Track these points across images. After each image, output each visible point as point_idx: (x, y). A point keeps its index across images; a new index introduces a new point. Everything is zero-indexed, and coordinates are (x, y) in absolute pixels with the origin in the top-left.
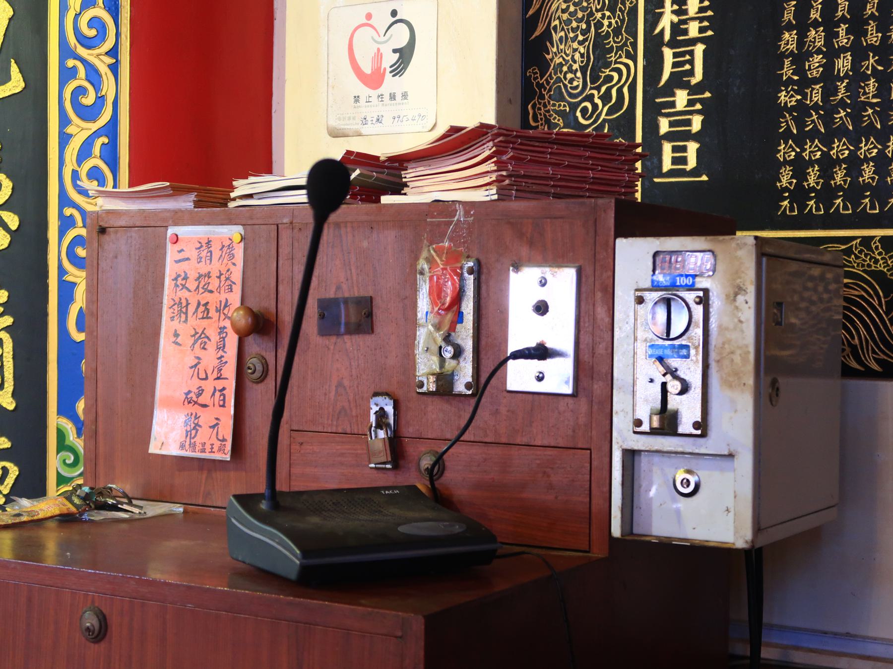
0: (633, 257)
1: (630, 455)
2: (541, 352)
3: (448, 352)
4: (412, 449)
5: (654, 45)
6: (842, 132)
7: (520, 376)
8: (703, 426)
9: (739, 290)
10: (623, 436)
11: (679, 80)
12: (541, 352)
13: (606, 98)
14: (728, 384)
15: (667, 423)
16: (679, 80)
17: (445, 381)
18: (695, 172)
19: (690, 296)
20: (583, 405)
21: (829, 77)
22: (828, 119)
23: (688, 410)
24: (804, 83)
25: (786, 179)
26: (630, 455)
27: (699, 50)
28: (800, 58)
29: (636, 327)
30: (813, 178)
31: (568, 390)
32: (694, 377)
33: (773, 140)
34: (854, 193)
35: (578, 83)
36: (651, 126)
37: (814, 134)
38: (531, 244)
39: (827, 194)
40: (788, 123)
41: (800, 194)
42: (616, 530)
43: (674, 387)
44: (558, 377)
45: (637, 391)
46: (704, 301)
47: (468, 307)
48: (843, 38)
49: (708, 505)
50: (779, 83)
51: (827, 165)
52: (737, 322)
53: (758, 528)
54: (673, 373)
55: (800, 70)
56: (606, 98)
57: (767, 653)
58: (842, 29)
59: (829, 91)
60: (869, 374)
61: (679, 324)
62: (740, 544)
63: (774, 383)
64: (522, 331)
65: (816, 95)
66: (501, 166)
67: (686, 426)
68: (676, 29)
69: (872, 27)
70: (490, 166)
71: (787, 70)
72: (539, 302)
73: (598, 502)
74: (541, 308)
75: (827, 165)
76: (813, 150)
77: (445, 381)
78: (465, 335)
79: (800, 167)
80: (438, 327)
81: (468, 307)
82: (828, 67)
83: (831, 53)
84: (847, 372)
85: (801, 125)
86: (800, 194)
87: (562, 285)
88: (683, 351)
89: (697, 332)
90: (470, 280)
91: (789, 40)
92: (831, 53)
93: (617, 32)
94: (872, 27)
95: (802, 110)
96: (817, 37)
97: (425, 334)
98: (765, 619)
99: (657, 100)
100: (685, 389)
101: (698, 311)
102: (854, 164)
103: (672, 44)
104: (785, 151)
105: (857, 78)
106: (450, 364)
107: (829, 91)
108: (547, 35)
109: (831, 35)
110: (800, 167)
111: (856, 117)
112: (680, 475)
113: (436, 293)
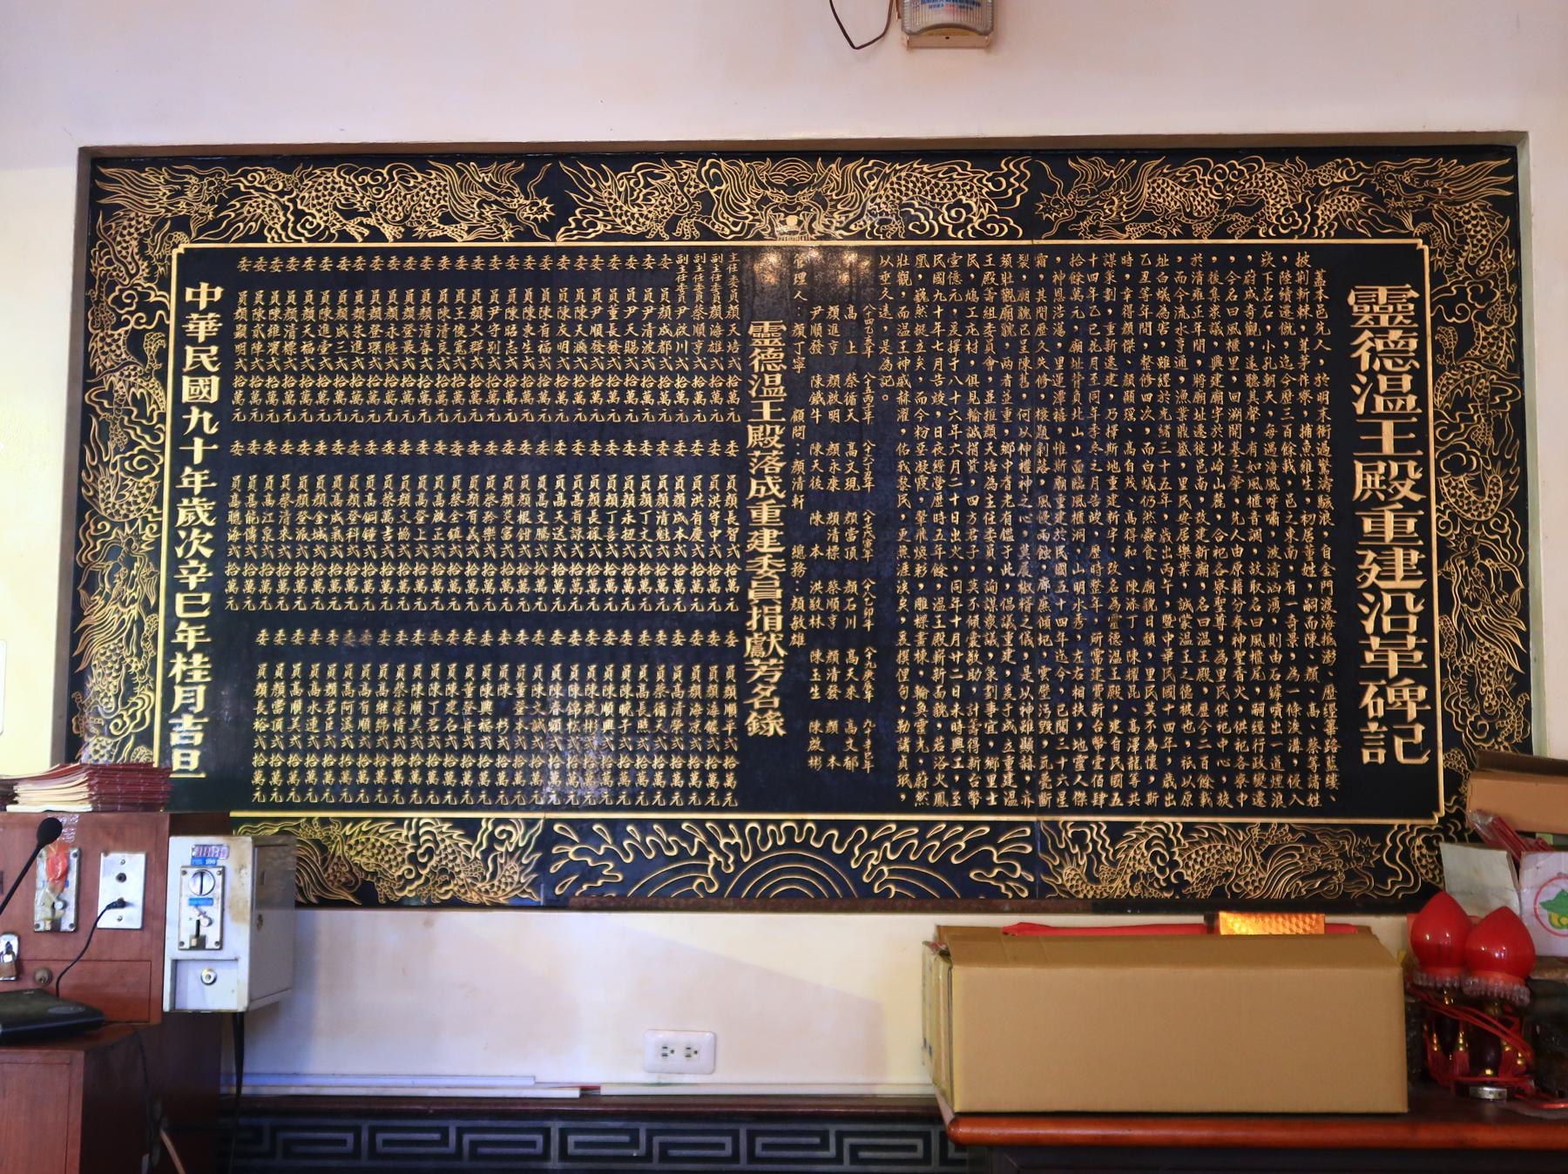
0: (181, 848)
1: (176, 962)
2: (121, 904)
3: (59, 905)
4: (28, 967)
5: (169, 684)
6: (294, 749)
7: (108, 921)
8: (220, 944)
9: (242, 867)
10: (172, 951)
11: (185, 708)
12: (121, 904)
13: (133, 717)
14: (235, 918)
15: (200, 943)
16: (185, 708)
17: (56, 924)
18: (197, 771)
19: (215, 871)
20: (147, 935)
21: (287, 714)
22: (286, 741)
23: (212, 935)
24: (271, 717)
25: (258, 778)
26: (176, 962)
27: (201, 690)
28: (269, 701)
29: (181, 887)
30: (276, 778)
31: (138, 925)
32: (216, 916)
33: (251, 752)
34: (303, 789)
35: (112, 705)
36: (165, 739)
37: (277, 750)
38: (116, 839)
39: (285, 789)
40: (260, 742)
41: (267, 789)
42: (166, 1007)
43: (204, 922)
44: (131, 918)
45: (180, 924)
46: (223, 873)
47: (72, 878)
48: (297, 690)
49: (221, 988)
50: (254, 716)
51: (285, 770)
52: (242, 884)
53: (251, 1000)
54: (203, 914)
55: (269, 708)
56: (133, 717)
57: (245, 1091)
58: (296, 685)
59: (288, 723)
60: (309, 905)
61: (208, 886)
62: (241, 1009)
63: (260, 918)
64: (108, 891)
65: (278, 725)
66: (91, 787)
67: (210, 944)
68: (185, 675)
69: (314, 685)
70: (84, 788)
71: (260, 708)
72: (121, 878)
73: (155, 993)
74: (122, 878)
75: (285, 770)
76: (277, 760)
77: (56, 924)
78: (70, 894)
79: (268, 771)
80: (53, 890)
81: (72, 878)
82: (287, 708)
83: (289, 699)
84: (299, 905)
85: (269, 743)
86: (267, 789)
87: (135, 864)
88: (210, 901)
89: (218, 891)
90: (74, 861)
91: (262, 689)
92: (289, 699)
93: (142, 672)
94: (314, 685)
95: (269, 735)
96: (279, 688)
97: (42, 893)
98: (246, 1069)
99: (233, 814)
100: (65, 905)
101: (219, 879)
102: (303, 770)
103: (182, 684)
104: (258, 760)
105: (305, 716)
106: (59, 912)
107: (288, 723)
108: (88, 669)
109: (289, 688)
110: (268, 771)
111: (304, 740)
112: (205, 973)
113: (51, 869)
